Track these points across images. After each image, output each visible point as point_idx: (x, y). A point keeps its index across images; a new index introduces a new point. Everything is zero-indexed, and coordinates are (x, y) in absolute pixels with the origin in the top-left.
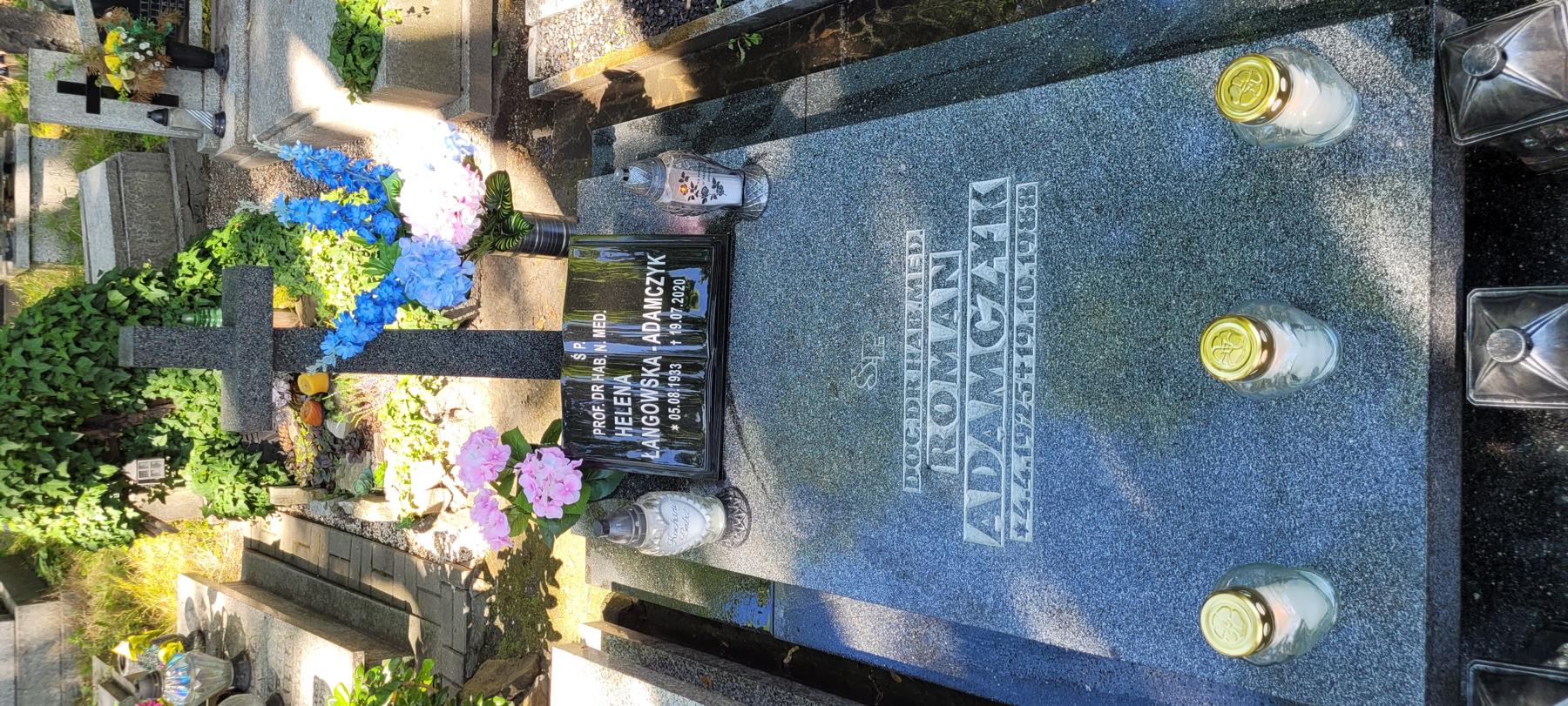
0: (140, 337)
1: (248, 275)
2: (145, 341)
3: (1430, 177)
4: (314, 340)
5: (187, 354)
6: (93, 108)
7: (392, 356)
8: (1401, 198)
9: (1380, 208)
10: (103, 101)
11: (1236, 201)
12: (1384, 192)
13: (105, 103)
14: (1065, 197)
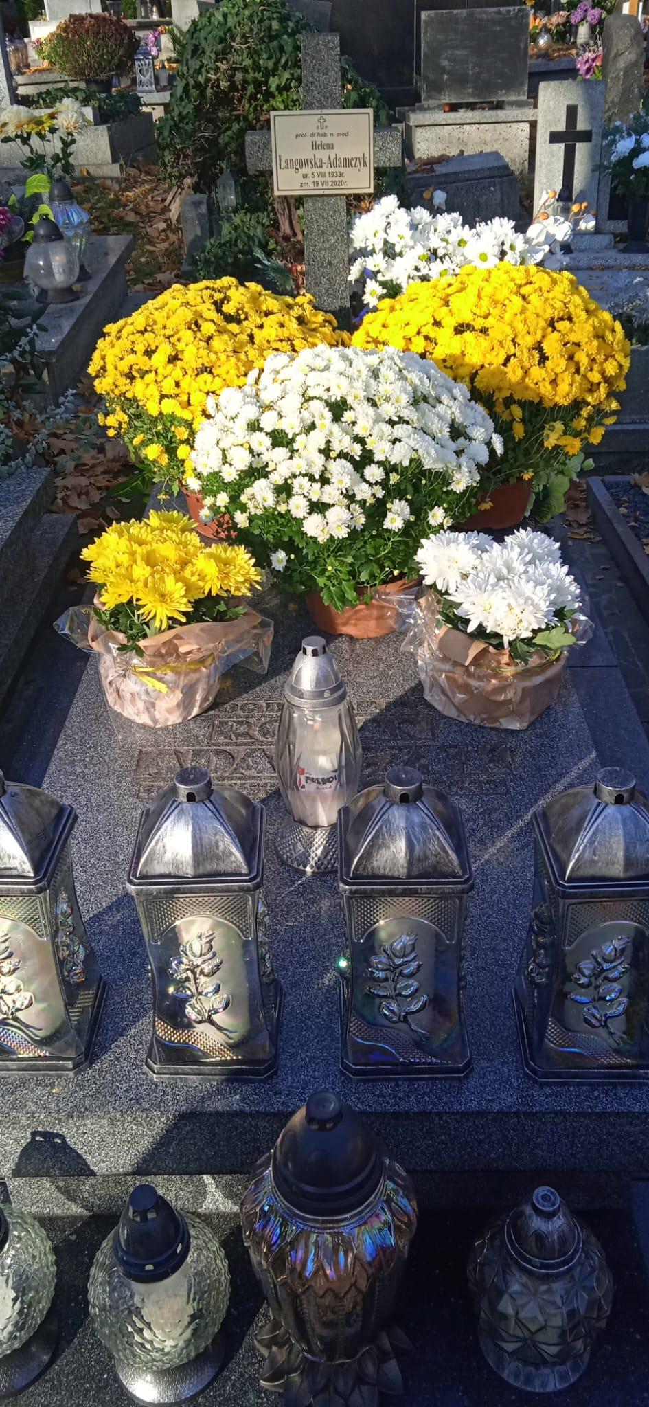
0: (329, 42)
1: (392, 142)
2: (326, 46)
3: (524, 1109)
4: (335, 212)
5: (316, 87)
6: (555, 137)
7: (324, 291)
8: (500, 1084)
9: (488, 1067)
10: (562, 146)
11: (494, 950)
12: (506, 1070)
13: (560, 148)
14: (494, 816)
